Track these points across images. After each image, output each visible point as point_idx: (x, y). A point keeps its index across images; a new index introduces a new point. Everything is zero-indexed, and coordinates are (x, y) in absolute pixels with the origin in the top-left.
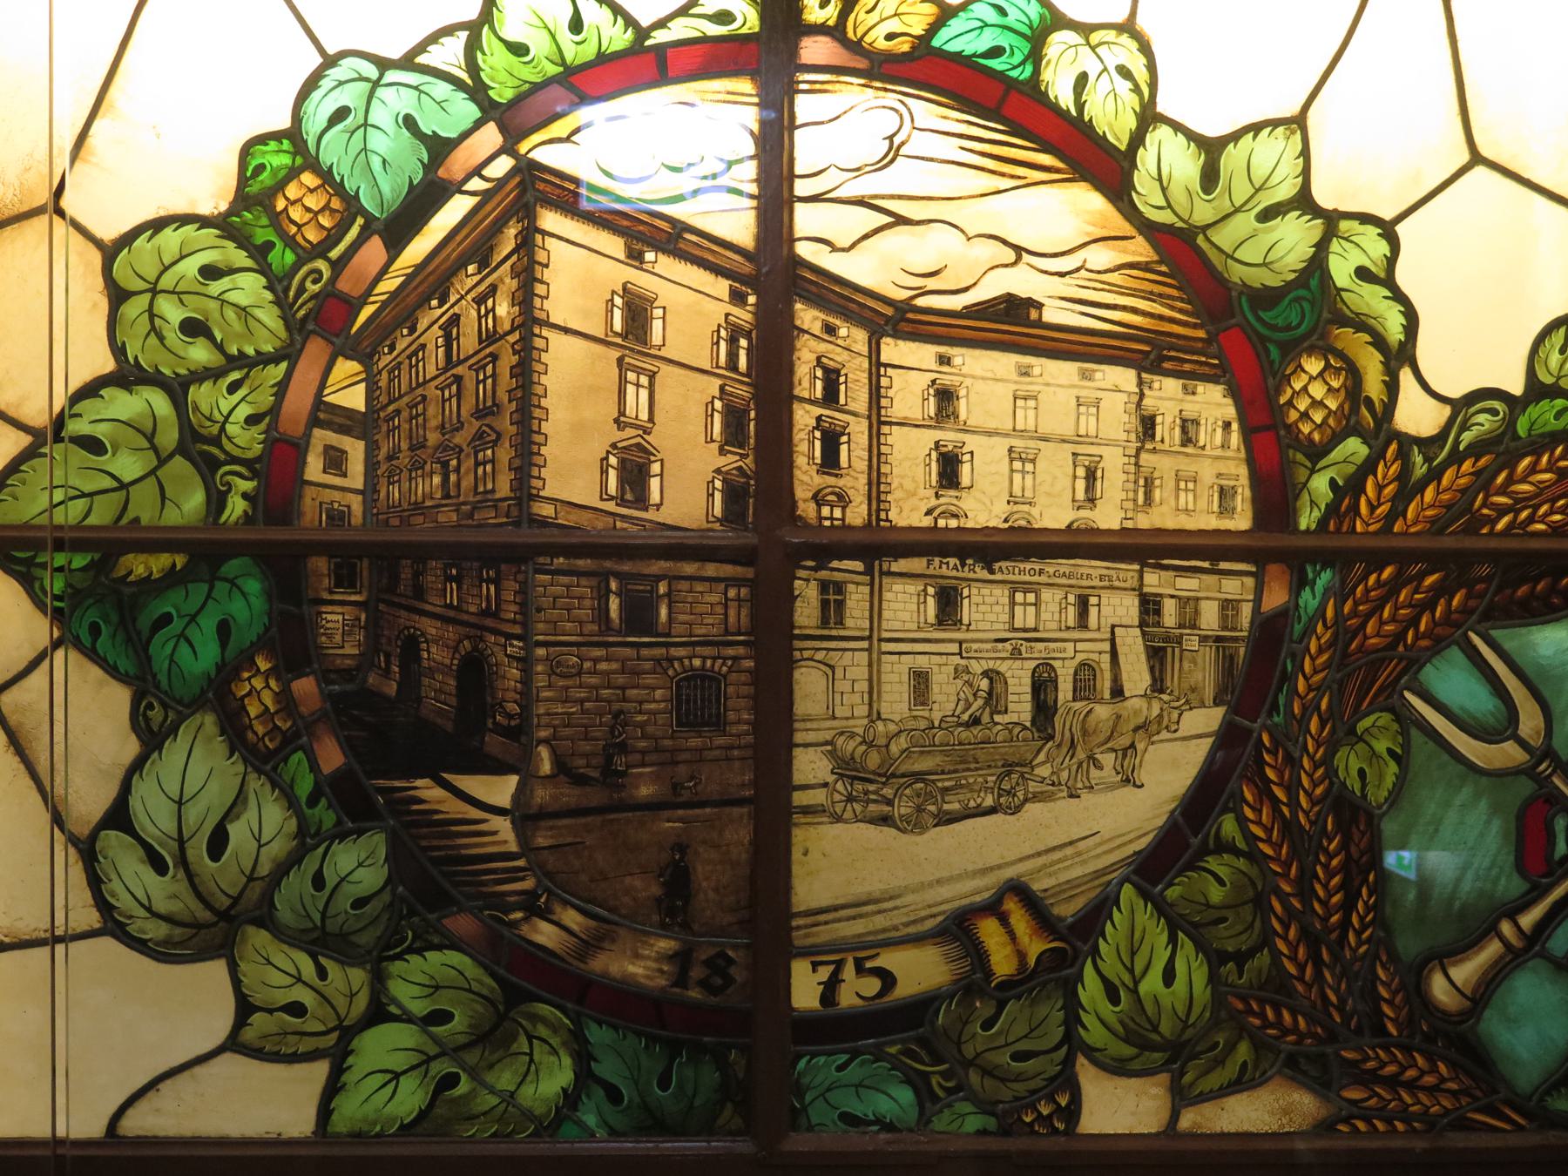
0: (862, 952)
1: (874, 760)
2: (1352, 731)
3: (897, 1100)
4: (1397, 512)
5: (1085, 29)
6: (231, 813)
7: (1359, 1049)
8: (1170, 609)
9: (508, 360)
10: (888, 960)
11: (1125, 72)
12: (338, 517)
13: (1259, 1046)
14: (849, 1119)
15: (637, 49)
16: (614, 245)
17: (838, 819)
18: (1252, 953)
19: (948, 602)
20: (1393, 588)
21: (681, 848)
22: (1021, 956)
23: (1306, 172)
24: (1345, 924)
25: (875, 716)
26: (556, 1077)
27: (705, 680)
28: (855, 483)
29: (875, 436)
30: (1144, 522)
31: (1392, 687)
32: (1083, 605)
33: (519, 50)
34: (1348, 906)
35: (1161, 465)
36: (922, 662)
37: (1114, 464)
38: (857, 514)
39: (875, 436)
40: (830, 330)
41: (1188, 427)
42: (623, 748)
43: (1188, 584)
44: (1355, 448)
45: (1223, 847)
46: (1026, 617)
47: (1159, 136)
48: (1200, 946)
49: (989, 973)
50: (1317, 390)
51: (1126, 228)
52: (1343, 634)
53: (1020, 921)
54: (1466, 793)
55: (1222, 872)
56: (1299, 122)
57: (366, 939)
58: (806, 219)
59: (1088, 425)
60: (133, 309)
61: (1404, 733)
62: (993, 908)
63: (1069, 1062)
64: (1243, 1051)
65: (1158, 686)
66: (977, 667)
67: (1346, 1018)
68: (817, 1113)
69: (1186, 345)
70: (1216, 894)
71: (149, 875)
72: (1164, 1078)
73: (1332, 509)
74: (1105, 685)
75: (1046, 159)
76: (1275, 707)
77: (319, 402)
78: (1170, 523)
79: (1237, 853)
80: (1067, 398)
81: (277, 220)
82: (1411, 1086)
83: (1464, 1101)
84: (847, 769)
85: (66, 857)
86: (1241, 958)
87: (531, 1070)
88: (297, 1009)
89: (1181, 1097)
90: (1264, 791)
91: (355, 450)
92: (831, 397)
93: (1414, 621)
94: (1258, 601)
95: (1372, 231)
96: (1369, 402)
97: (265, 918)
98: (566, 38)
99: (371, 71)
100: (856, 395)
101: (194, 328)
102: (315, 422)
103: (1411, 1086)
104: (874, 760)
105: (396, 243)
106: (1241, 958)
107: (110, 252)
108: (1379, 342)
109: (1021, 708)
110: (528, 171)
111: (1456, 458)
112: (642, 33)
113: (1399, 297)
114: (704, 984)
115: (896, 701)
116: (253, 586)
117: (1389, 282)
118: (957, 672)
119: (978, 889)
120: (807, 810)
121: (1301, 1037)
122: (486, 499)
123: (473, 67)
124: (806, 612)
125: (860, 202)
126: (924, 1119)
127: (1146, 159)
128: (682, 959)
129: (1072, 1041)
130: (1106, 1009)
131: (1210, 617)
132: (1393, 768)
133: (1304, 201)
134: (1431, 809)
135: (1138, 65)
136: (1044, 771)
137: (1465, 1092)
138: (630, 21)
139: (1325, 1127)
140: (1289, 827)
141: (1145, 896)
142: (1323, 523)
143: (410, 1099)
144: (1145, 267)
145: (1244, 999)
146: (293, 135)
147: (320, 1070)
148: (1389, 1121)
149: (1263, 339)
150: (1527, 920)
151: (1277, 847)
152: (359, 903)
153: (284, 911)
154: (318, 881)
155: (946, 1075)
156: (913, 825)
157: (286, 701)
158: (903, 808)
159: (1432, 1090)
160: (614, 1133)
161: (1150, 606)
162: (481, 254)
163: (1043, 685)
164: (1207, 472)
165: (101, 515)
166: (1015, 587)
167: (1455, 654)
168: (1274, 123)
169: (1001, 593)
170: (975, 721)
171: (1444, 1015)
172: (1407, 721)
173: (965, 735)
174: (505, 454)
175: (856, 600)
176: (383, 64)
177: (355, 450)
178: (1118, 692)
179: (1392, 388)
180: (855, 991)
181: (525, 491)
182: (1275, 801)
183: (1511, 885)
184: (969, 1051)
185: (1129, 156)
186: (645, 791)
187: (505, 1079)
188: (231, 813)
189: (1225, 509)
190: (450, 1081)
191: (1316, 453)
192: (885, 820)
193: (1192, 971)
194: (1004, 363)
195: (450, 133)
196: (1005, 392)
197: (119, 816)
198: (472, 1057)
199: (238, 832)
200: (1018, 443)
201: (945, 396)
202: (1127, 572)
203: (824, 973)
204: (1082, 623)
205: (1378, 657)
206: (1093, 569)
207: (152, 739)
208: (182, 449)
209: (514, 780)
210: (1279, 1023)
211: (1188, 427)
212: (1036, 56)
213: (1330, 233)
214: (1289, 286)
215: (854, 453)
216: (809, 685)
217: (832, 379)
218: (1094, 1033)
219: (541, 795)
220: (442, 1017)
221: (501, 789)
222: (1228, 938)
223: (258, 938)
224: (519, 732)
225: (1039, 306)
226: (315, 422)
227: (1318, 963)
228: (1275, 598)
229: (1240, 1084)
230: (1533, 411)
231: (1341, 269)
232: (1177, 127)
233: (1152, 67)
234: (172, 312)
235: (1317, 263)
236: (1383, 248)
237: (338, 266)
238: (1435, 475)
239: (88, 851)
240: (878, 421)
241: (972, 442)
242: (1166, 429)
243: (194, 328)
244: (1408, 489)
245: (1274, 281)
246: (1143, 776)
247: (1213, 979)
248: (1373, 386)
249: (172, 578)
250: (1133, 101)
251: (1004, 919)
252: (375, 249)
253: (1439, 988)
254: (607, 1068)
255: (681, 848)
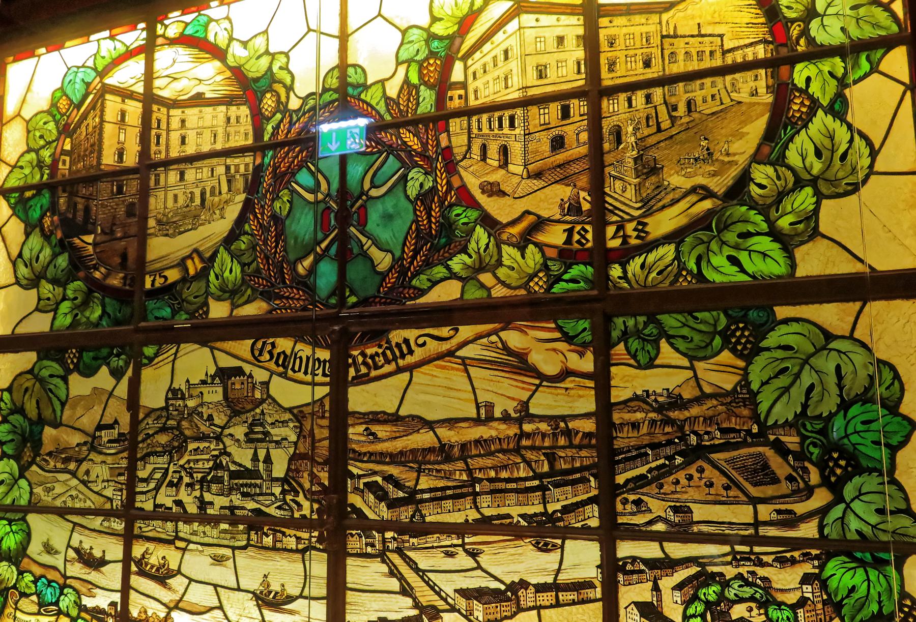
0: (160, 272)
1: (165, 219)
2: (278, 196)
3: (166, 312)
4: (289, 131)
5: (216, 21)
6: (40, 251)
7: (279, 289)
8: (232, 168)
9: (98, 132)
10: (166, 273)
11: (226, 29)
12: (64, 176)
13: (253, 290)
14: (157, 318)
15: (127, 51)
16: (119, 99)
17: (157, 236)
18: (253, 262)
19: (182, 174)
20: (287, 153)
21: (126, 249)
22: (196, 269)
23: (268, 45)
24: (276, 252)
25: (165, 208)
26: (98, 312)
27: (133, 204)
28: (163, 148)
29: (168, 134)
30: (227, 146)
31: (289, 182)
32: (212, 170)
33: (103, 58)
34: (276, 247)
35: (231, 130)
36: (176, 192)
37: (220, 132)
38: (163, 156)
39: (168, 134)
40: (159, 110)
41: (238, 118)
42: (114, 224)
43: (237, 161)
44: (279, 116)
45: (246, 233)
46: (199, 176)
47: (234, 43)
48: (239, 262)
49: (188, 274)
50: (270, 102)
51: (226, 69)
52: (275, 168)
53: (197, 260)
54: (306, 210)
55: (245, 240)
56: (266, 32)
57: (63, 280)
58: (157, 83)
59: (215, 123)
60: (31, 135)
61: (292, 195)
62: (190, 257)
63: (206, 298)
64: (249, 292)
65: (230, 190)
66: (188, 191)
67: (276, 280)
68: (150, 317)
69: (238, 97)
70: (243, 247)
71: (24, 268)
72: (229, 301)
73: (273, 134)
74: (217, 192)
75: (207, 56)
76: (258, 192)
77: (62, 150)
78: (233, 145)
79: (249, 234)
80: (210, 116)
81: (58, 108)
82: (292, 299)
83: (307, 302)
84: (159, 222)
85: (10, 265)
86: (249, 264)
87: (92, 312)
88: (48, 299)
89: (234, 306)
90: (255, 216)
91: (67, 159)
92: (159, 127)
93: (293, 162)
94: (254, 163)
95: (283, 56)
96: (282, 103)
97: (45, 278)
98: (113, 52)
99: (75, 69)
100: (164, 125)
101: (41, 137)
102: (61, 154)
103: (292, 299)
104: (165, 219)
105: (78, 110)
106: (249, 264)
107: (28, 122)
108: (285, 86)
109: (198, 201)
110: (104, 85)
111: (304, 114)
112: (128, 47)
113: (290, 72)
114: (129, 285)
115: (170, 203)
116: (47, 195)
117: (287, 69)
118: (184, 193)
119: (186, 252)
120: (150, 235)
121: (265, 286)
122: (92, 166)
123: (95, 64)
124: (152, 183)
125: (167, 76)
126: (173, 316)
127: (230, 50)
128: (124, 278)
129: (207, 293)
130: (216, 282)
131: (242, 169)
132: (288, 205)
133: (267, 52)
134: (298, 215)
135: (228, 26)
136: (203, 217)
137: (306, 299)
138: (125, 45)
139: (270, 312)
140: (261, 226)
141: (226, 249)
142: (270, 139)
143: (68, 320)
144: (229, 78)
145: (250, 276)
146: (62, 88)
147: (51, 314)
148: (286, 309)
149: (256, 91)
150: (323, 245)
151: (258, 231)
152: (62, 271)
153: (49, 275)
154: (55, 266)
155: (179, 304)
156: (173, 236)
157: (52, 222)
158: (171, 232)
159: (298, 299)
160: (109, 326)
161: (228, 168)
162: (94, 108)
163: (203, 194)
164: (242, 130)
165: (22, 183)
166: (197, 168)
167: (304, 170)
168: (259, 34)
169: (194, 171)
170: (188, 206)
171: (301, 276)
172: (293, 192)
173: (185, 209)
174: (95, 155)
175: (162, 177)
176: (78, 67)
177: (67, 159)
178: (220, 193)
179: (288, 98)
180: (159, 282)
181: (99, 163)
182: (258, 218)
183: (320, 235)
184: (184, 297)
185: (226, 51)
186: (119, 235)
187: (87, 314)
188: (40, 251)
189: (246, 139)
190: (77, 315)
191: (268, 119)
192: (167, 235)
193: (237, 269)
194: (195, 110)
195: (90, 81)
196: (196, 118)
197: (20, 255)
198: (81, 308)
199: (41, 256)
200: (199, 130)
201: (183, 121)
202: (222, 160)
203: (152, 278)
204: (212, 176)
205: (284, 174)
206: (215, 161)
207: (27, 235)
208: (37, 165)
209: (93, 236)
210: (258, 283)
211: (238, 118)
212: (206, 30)
213: (273, 59)
214: (263, 75)
215: (163, 140)
216: (152, 200)
217: (159, 121)
218: (213, 289)
219: (98, 238)
220: (76, 298)
221: (89, 239)
222: (246, 259)
223: (43, 282)
224: (94, 224)
225: (204, 94)
226: (61, 154)
227: (269, 264)
228: (258, 161)
229: (247, 302)
230: (324, 96)
231: (275, 69)
232: (238, 40)
233: (232, 27)
234: (38, 134)
235: (270, 68)
236: (286, 60)
237: (68, 117)
238: (298, 120)
239: (14, 264)
240: (168, 131)
241: (189, 132)
242: (233, 120)
243: (41, 137)
244: (291, 124)
245: (259, 75)
246: (226, 215)
247: (242, 271)
248: (283, 99)
249: (34, 196)
250: (227, 36)
251: (193, 259)
252: (75, 111)
253: (301, 269)
254: (109, 310)
255: (126, 249)
